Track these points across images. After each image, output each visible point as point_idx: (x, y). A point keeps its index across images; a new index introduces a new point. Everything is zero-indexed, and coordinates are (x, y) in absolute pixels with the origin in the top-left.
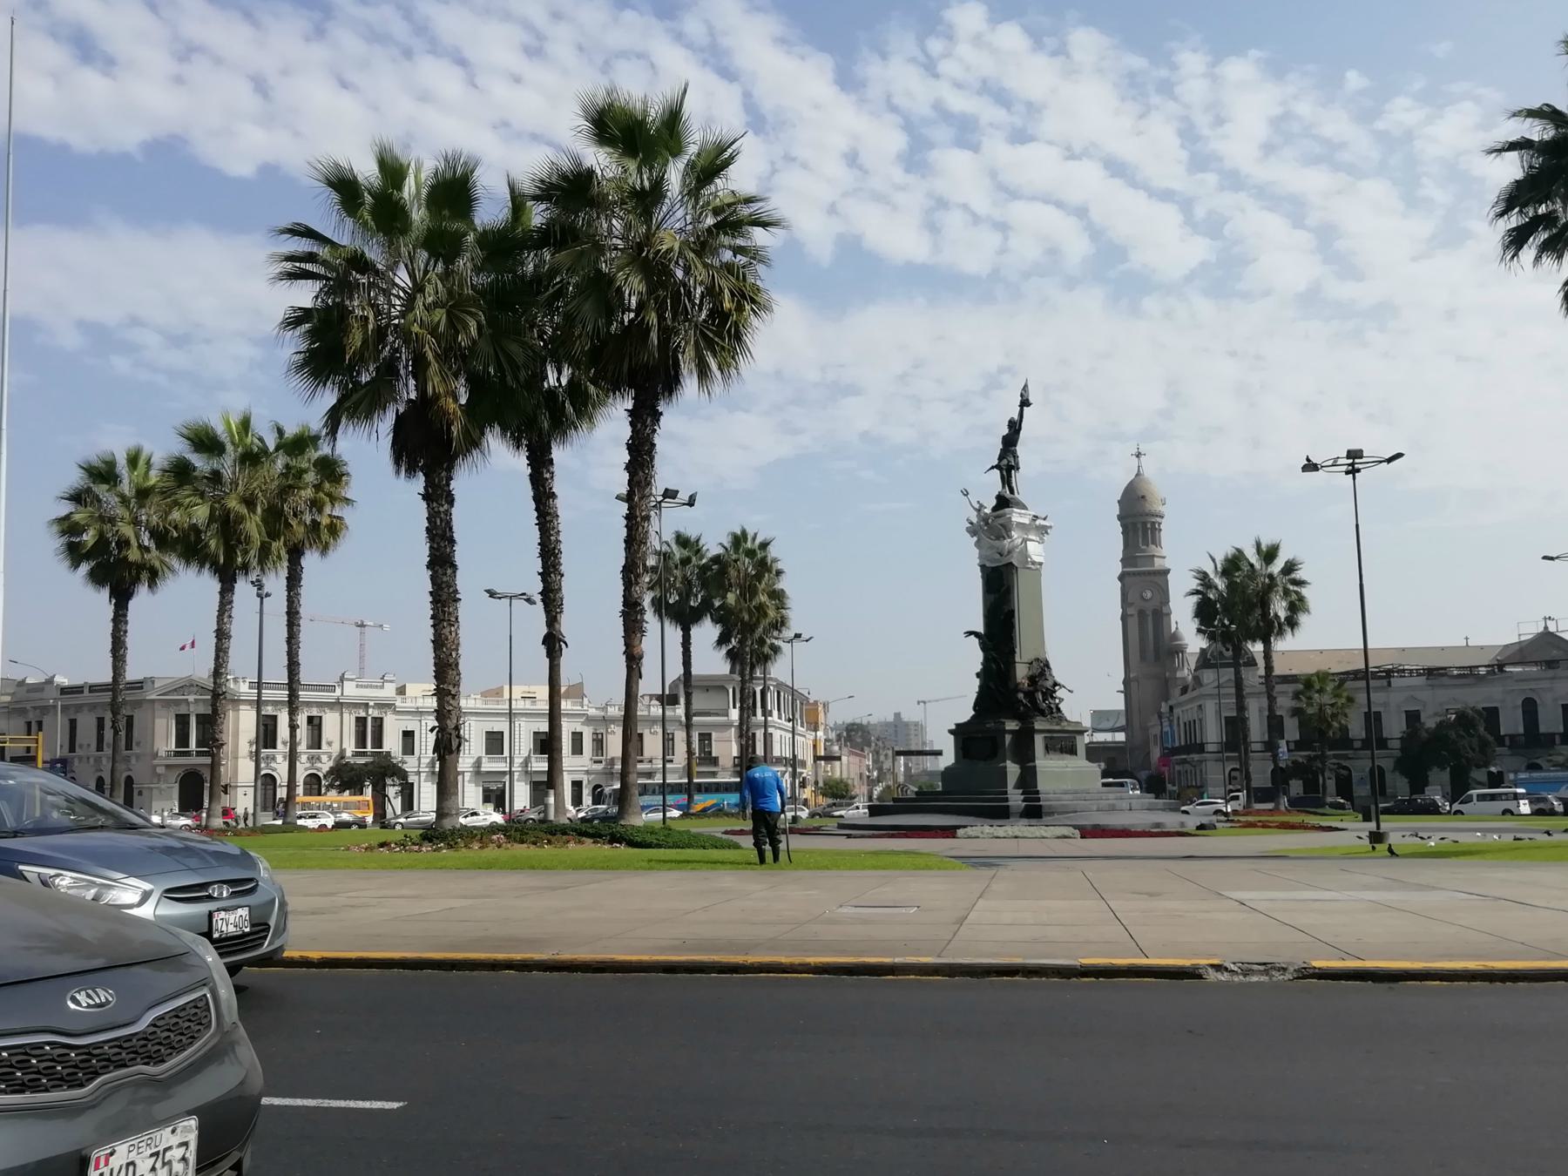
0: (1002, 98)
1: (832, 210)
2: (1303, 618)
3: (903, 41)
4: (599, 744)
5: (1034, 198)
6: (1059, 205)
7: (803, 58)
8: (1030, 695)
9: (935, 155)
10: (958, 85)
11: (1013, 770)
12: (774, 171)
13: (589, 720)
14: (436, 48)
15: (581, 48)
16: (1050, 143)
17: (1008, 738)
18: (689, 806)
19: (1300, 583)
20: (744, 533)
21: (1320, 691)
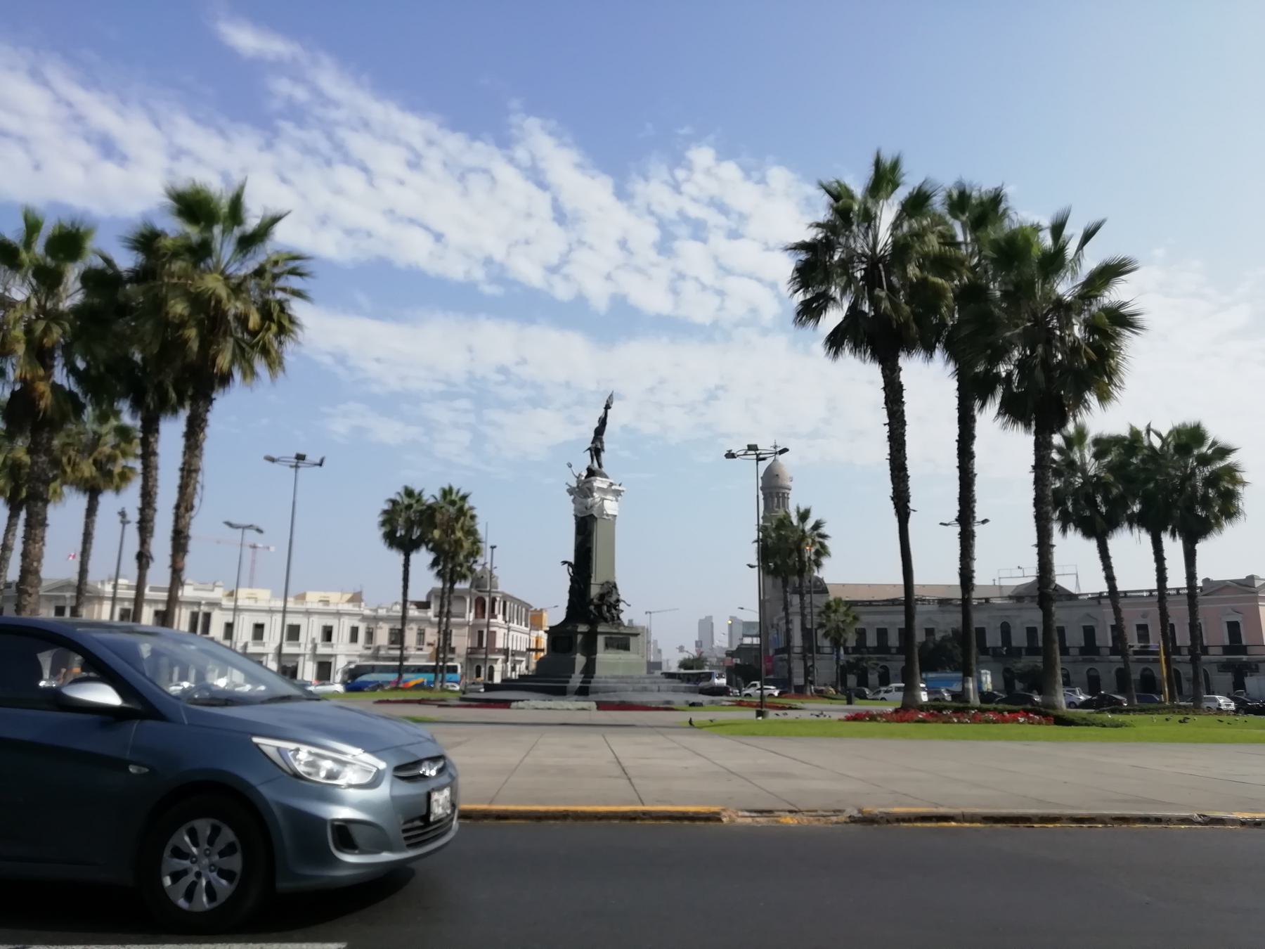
0: (723, 209)
1: (608, 277)
2: (824, 560)
3: (659, 171)
4: (370, 635)
5: (742, 275)
6: (759, 280)
7: (593, 178)
8: (598, 607)
9: (677, 245)
10: (695, 200)
11: (580, 660)
12: (570, 250)
13: (364, 618)
14: (347, 159)
15: (445, 164)
16: (754, 240)
17: (580, 637)
18: (398, 682)
19: (824, 536)
20: (451, 489)
21: (835, 611)
